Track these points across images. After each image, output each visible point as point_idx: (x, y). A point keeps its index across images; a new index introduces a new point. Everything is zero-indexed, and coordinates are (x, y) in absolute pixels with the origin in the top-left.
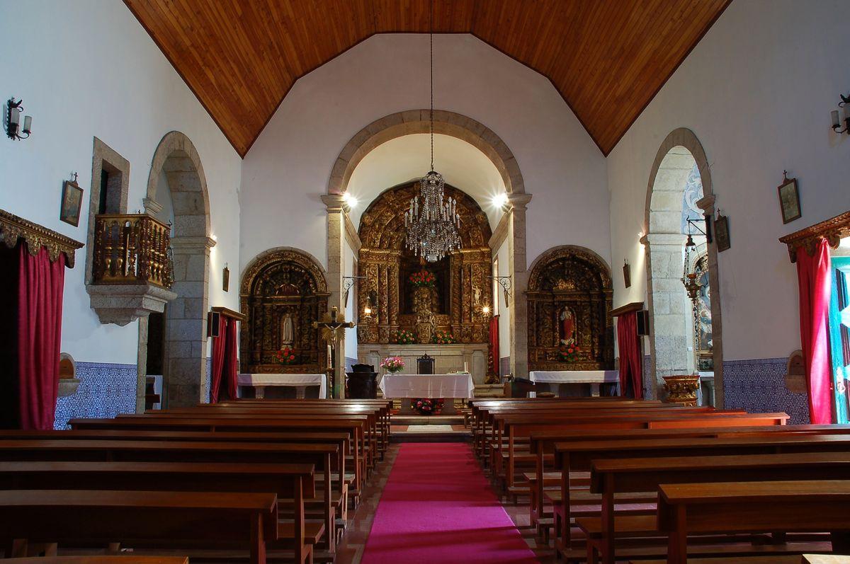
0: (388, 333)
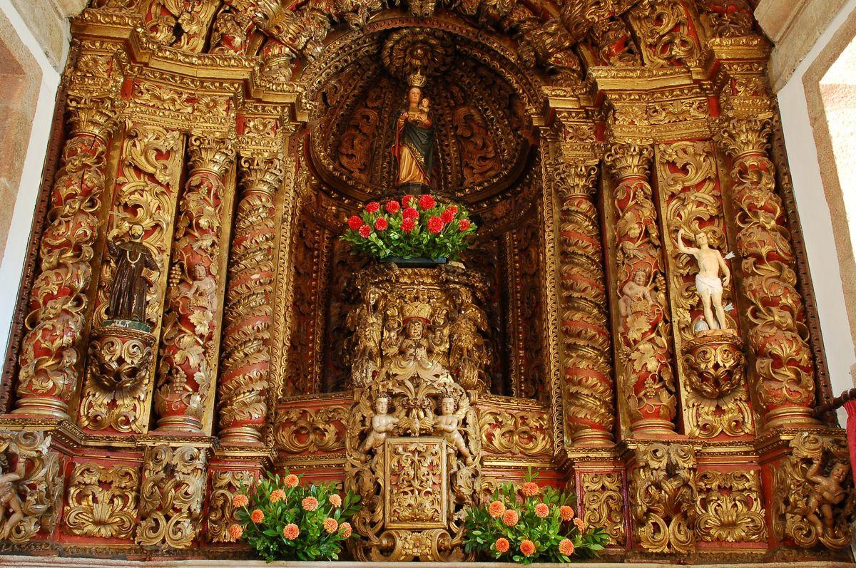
0: (196, 485)
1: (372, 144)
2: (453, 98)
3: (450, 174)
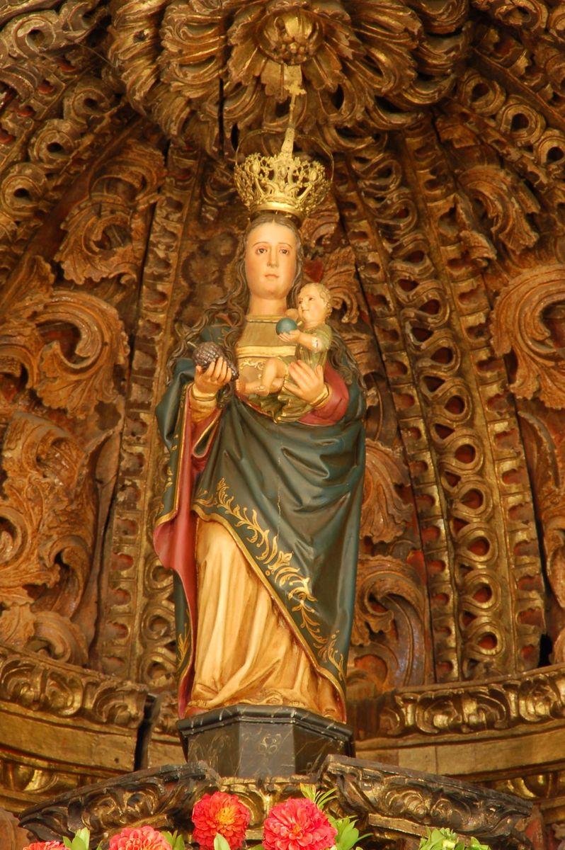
1: (95, 458)
2: (483, 221)
3: (485, 592)
